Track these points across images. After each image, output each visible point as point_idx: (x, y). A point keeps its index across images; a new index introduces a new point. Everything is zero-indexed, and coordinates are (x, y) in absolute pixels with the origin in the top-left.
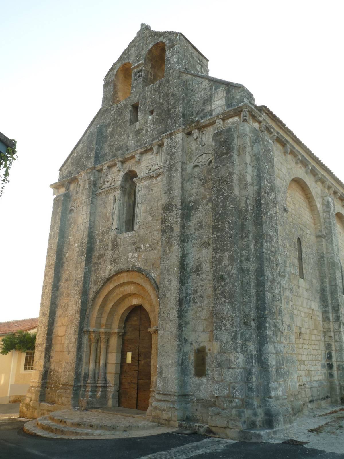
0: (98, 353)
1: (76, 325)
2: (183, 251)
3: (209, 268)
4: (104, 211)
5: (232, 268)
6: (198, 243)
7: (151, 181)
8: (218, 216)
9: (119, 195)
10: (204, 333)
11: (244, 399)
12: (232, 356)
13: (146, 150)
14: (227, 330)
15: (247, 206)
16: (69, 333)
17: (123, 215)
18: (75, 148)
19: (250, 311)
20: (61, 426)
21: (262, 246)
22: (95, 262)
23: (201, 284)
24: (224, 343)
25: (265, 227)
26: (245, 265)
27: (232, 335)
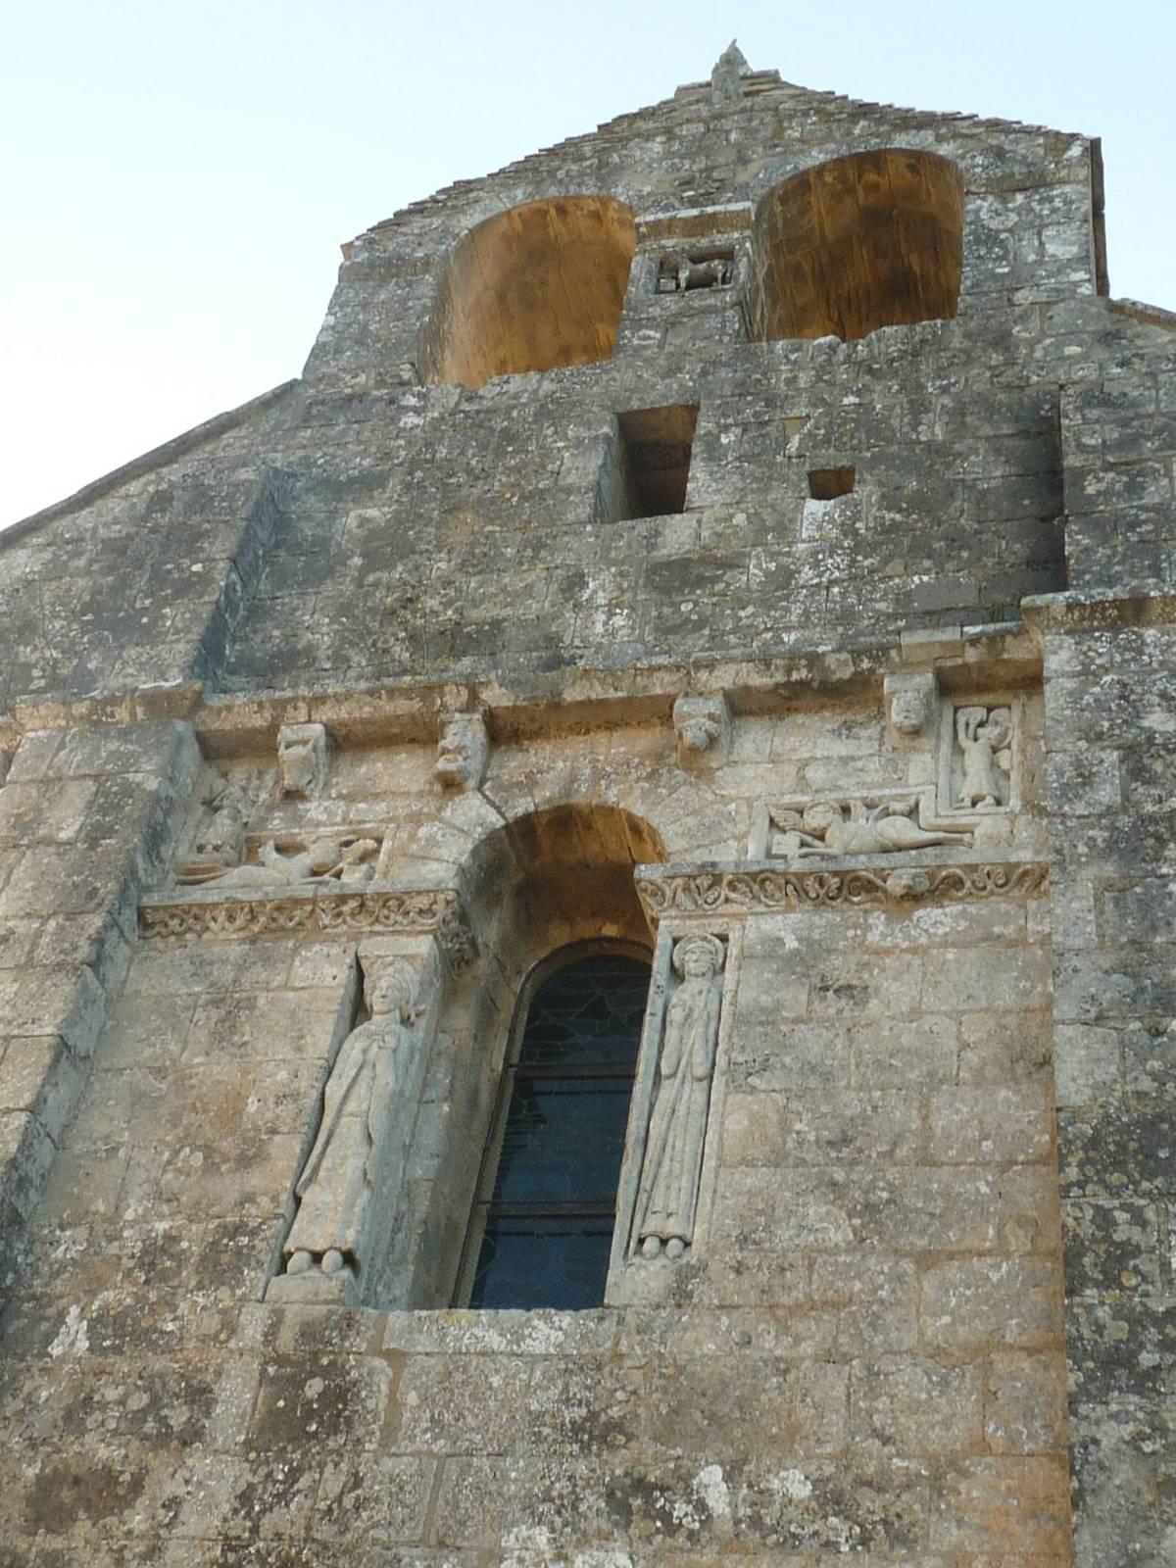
4: (213, 1070)
9: (411, 975)
18: (185, 445)
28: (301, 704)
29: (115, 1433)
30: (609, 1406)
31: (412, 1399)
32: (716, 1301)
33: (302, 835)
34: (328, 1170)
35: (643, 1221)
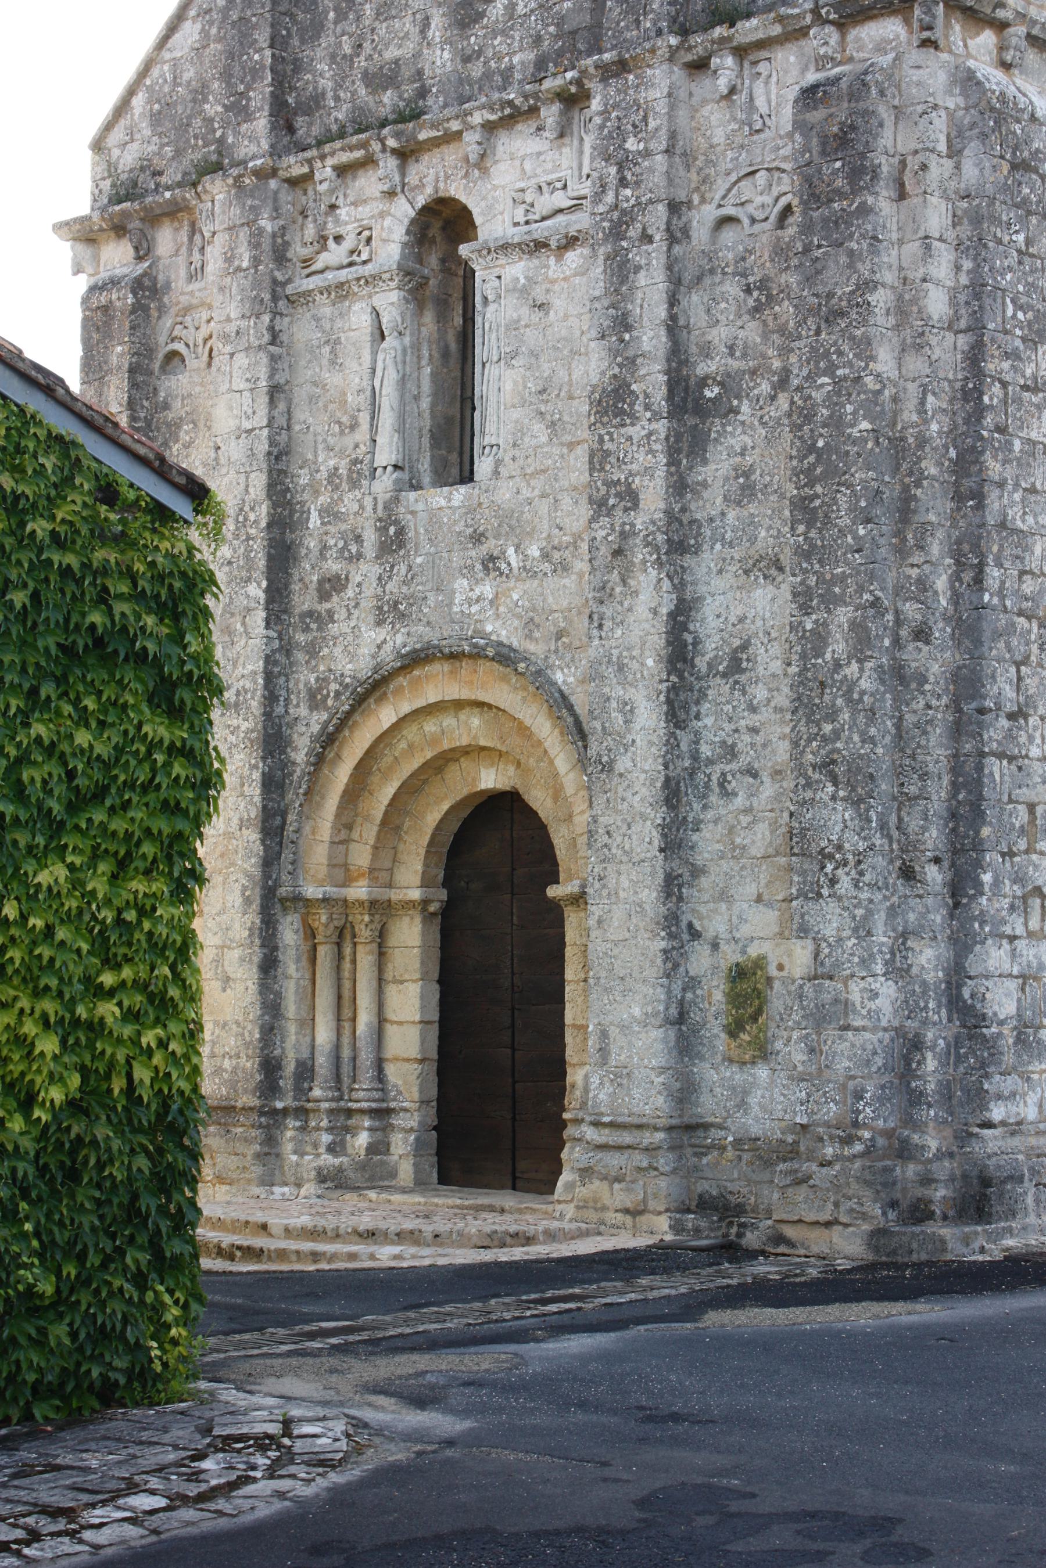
0: (347, 984)
1: (249, 876)
2: (679, 587)
3: (779, 663)
5: (862, 670)
6: (737, 557)
7: (536, 262)
8: (812, 459)
10: (761, 907)
11: (894, 1130)
12: (856, 989)
13: (511, 116)
14: (840, 899)
15: (926, 422)
16: (219, 906)
17: (417, 398)
19: (924, 829)
20: (258, 1242)
21: (979, 580)
22: (306, 607)
23: (751, 724)
24: (830, 945)
25: (994, 502)
26: (915, 655)
27: (854, 918)
31: (422, 531)
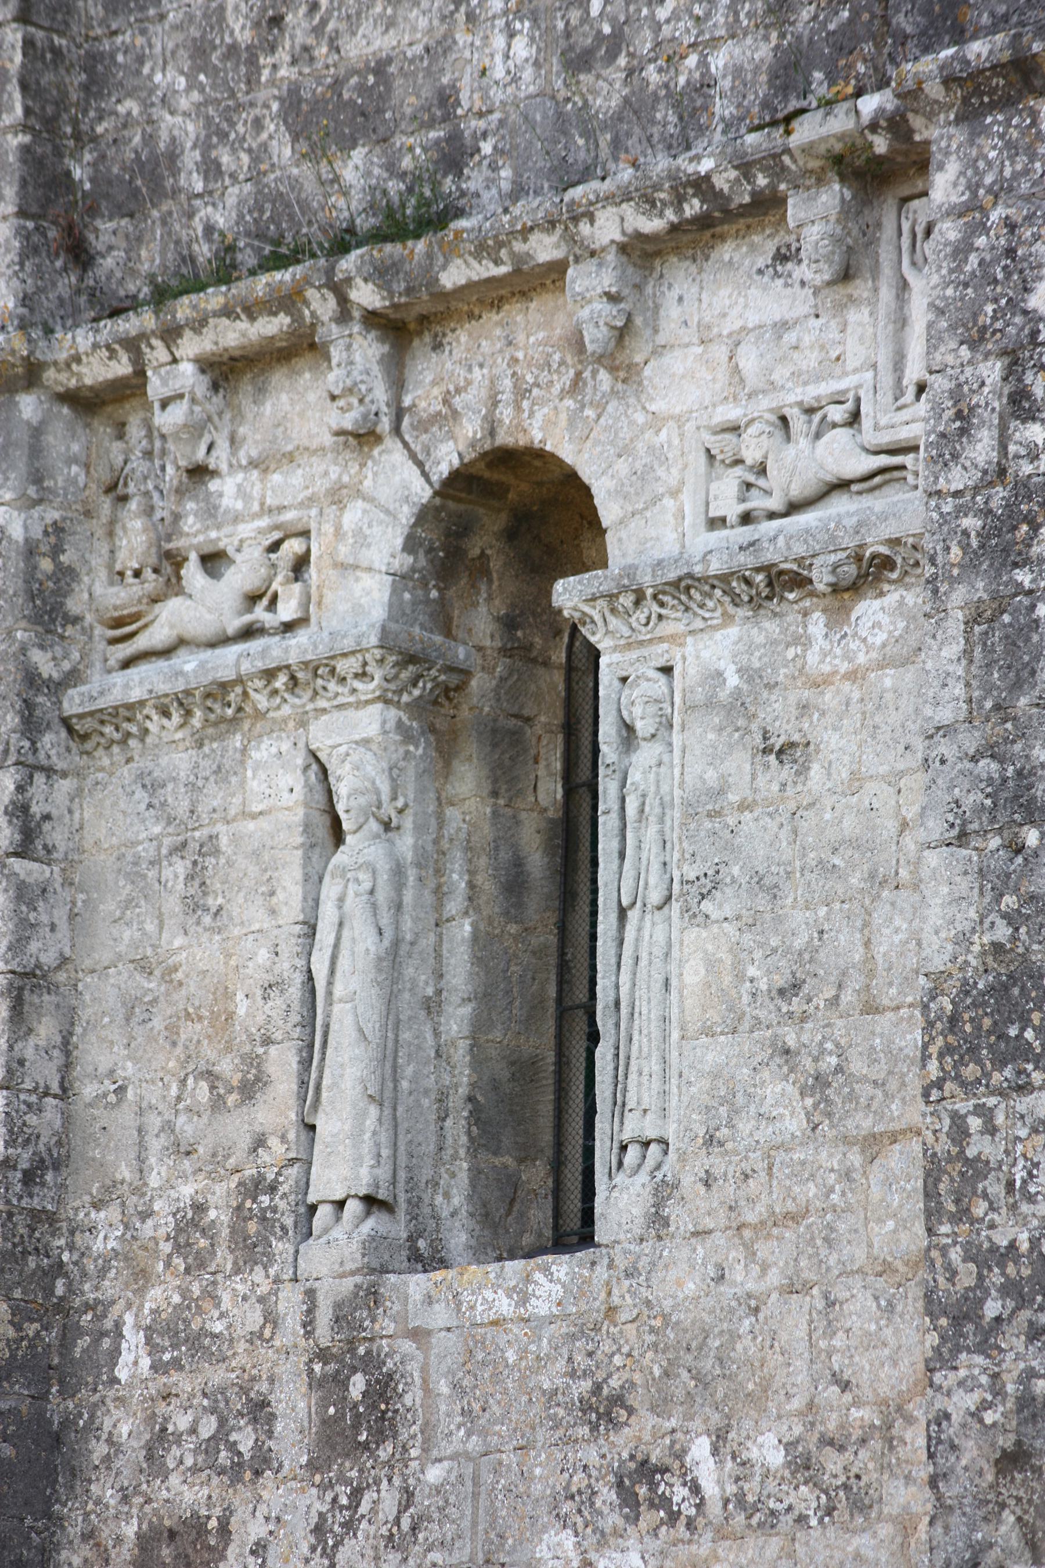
7: (771, 627)
13: (703, 222)
17: (432, 1006)
28: (155, 342)
29: (195, 1470)
30: (610, 1375)
32: (690, 1227)
33: (223, 538)
34: (330, 1088)
35: (622, 1123)
